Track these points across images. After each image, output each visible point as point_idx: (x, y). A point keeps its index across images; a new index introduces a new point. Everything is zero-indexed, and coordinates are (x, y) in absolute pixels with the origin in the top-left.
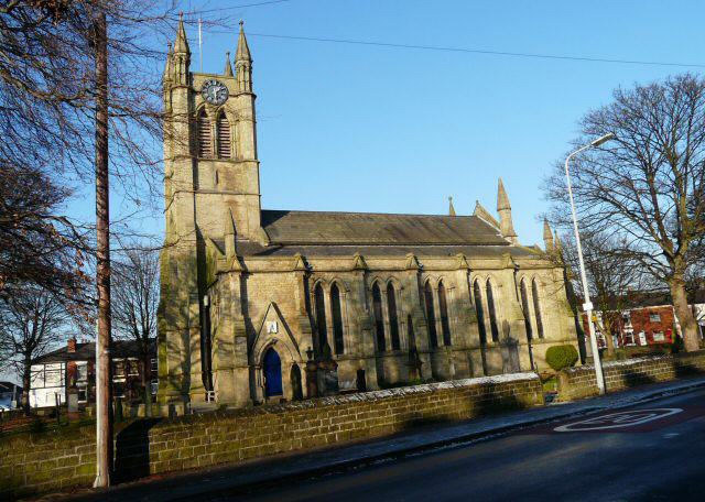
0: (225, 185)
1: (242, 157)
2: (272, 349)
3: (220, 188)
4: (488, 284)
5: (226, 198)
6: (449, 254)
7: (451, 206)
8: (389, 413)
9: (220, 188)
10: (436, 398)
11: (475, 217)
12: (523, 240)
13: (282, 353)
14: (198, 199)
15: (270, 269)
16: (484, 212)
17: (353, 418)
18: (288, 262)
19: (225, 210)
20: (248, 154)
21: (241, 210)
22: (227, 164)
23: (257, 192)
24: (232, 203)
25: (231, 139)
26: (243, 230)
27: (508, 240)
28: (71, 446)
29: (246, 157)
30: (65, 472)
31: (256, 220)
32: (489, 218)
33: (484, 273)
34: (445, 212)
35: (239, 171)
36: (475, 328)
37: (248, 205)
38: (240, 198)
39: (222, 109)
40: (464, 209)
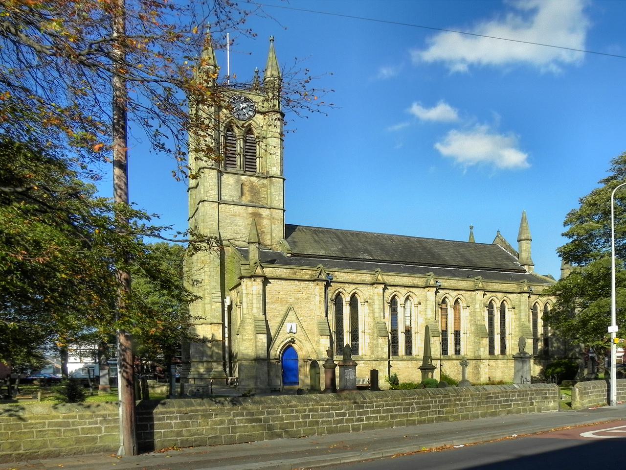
0: (249, 198)
1: (268, 172)
2: (290, 346)
3: (246, 200)
4: (456, 302)
5: (250, 210)
6: (468, 276)
7: (471, 234)
8: (414, 409)
9: (246, 200)
10: (460, 400)
11: (493, 245)
12: (537, 270)
13: (412, 363)
14: (280, 211)
15: (294, 277)
16: (504, 242)
17: (378, 412)
18: (310, 272)
19: (250, 221)
20: (275, 170)
21: (265, 222)
22: (252, 179)
23: (281, 206)
24: (256, 216)
25: (257, 156)
26: (267, 240)
27: (526, 267)
28: (397, 456)
29: (272, 173)
30: (87, 440)
31: (278, 232)
32: (508, 247)
33: (500, 295)
34: (466, 239)
35: (264, 186)
36: (486, 341)
37: (272, 218)
38: (265, 212)
39: (250, 124)
40: (484, 237)
